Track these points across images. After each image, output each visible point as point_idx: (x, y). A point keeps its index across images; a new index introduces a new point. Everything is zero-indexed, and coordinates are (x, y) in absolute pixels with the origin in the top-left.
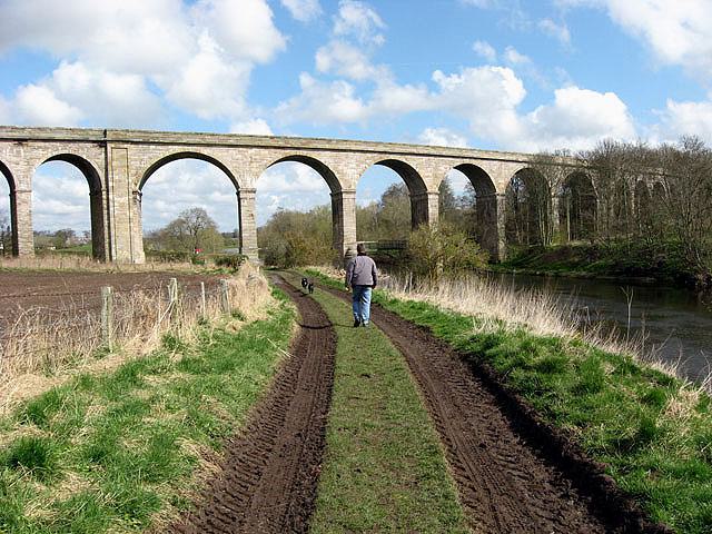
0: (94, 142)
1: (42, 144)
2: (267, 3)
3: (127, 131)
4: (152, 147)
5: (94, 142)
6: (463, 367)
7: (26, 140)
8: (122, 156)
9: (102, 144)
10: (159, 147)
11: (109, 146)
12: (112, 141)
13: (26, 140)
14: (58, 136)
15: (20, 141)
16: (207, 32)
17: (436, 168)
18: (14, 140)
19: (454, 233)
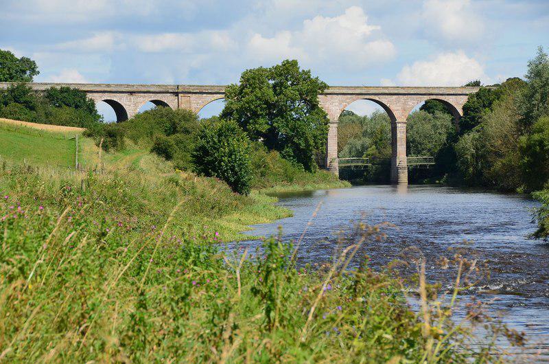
0: (171, 93)
1: (142, 94)
2: (537, 72)
3: (191, 86)
4: (205, 95)
5: (171, 93)
6: (148, 308)
7: (135, 92)
8: (187, 101)
9: (176, 94)
10: (209, 95)
11: (180, 95)
12: (181, 93)
13: (135, 92)
14: (152, 90)
15: (131, 93)
16: (538, 193)
17: (405, 104)
18: (128, 92)
19: (444, 286)
